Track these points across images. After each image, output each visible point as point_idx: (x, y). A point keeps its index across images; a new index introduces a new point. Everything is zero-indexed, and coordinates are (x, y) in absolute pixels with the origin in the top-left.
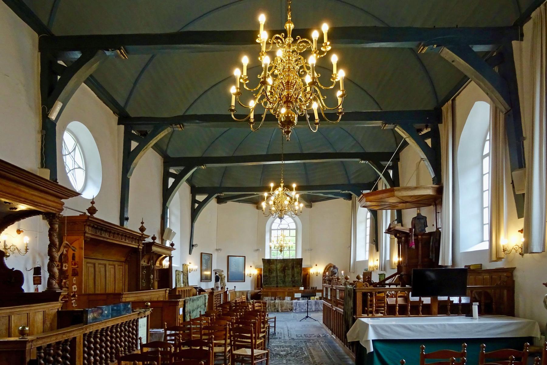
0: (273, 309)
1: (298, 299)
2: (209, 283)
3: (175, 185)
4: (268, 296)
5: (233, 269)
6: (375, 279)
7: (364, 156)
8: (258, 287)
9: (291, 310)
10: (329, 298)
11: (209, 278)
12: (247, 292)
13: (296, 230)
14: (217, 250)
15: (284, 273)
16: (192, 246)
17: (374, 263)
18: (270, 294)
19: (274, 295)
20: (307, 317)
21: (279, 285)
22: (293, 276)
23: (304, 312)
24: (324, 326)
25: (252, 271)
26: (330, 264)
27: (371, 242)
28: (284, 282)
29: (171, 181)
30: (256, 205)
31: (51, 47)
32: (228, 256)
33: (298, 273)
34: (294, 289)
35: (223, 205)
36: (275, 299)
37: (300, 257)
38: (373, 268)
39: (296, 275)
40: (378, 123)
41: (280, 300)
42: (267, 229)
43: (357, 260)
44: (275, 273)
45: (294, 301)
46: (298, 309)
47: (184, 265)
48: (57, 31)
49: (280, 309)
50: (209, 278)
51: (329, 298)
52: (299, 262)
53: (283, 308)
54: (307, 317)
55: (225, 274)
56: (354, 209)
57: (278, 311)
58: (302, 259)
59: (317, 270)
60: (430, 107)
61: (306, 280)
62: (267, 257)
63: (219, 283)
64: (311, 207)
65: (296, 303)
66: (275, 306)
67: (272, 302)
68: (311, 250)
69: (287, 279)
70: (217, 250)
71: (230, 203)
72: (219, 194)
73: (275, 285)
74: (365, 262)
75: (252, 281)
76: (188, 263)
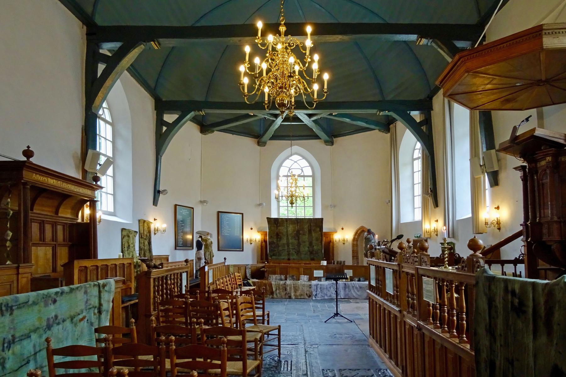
0: (283, 294)
1: (319, 279)
2: (190, 252)
3: (107, 73)
4: (275, 273)
5: (225, 232)
6: (434, 251)
7: (422, 30)
8: (262, 259)
9: (310, 296)
10: (390, 290)
11: (189, 244)
12: (246, 267)
13: (313, 176)
14: (202, 202)
15: (298, 239)
16: (157, 193)
17: (434, 224)
18: (278, 270)
19: (285, 272)
20: (337, 314)
21: (291, 258)
22: (311, 244)
23: (331, 300)
24: (372, 341)
25: (253, 235)
26: (362, 227)
27: (425, 191)
28: (298, 252)
29: (101, 67)
30: (256, 140)
31: (95, 34)
32: (219, 212)
33: (317, 240)
34: (313, 264)
35: (209, 136)
36: (286, 279)
37: (320, 217)
38: (429, 233)
39: (314, 242)
40: (413, 37)
41: (293, 279)
42: (273, 174)
43: (402, 221)
44: (285, 238)
45: (314, 283)
46: (319, 296)
47: (143, 223)
48: (99, 21)
49: (293, 294)
50: (189, 244)
51: (390, 290)
52: (318, 223)
53: (298, 293)
54: (337, 314)
55: (214, 239)
56: (394, 144)
57: (290, 297)
58: (322, 219)
59: (343, 236)
60: (422, 97)
61: (328, 250)
62: (274, 215)
63: (202, 252)
64: (332, 143)
65: (317, 285)
66: (286, 290)
67: (282, 282)
68: (335, 206)
69: (302, 249)
70: (202, 202)
71: (217, 135)
72: (197, 113)
73: (286, 257)
74: (419, 224)
75: (253, 250)
76: (151, 220)
